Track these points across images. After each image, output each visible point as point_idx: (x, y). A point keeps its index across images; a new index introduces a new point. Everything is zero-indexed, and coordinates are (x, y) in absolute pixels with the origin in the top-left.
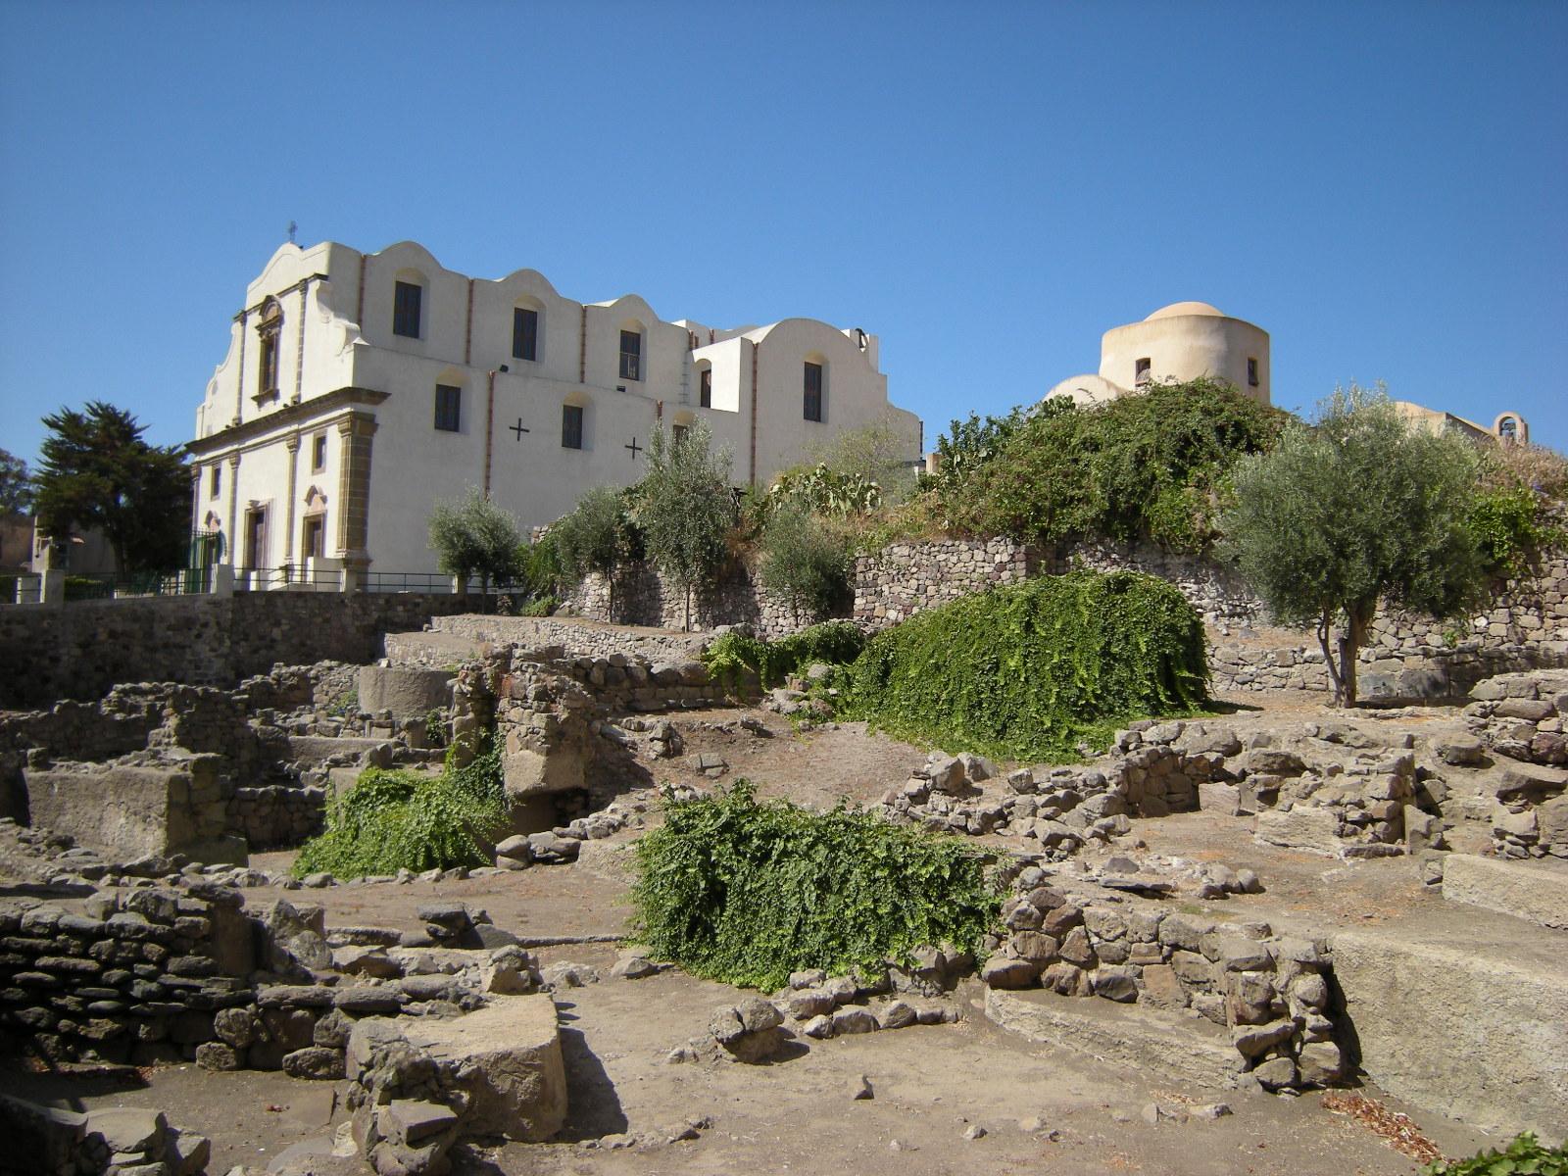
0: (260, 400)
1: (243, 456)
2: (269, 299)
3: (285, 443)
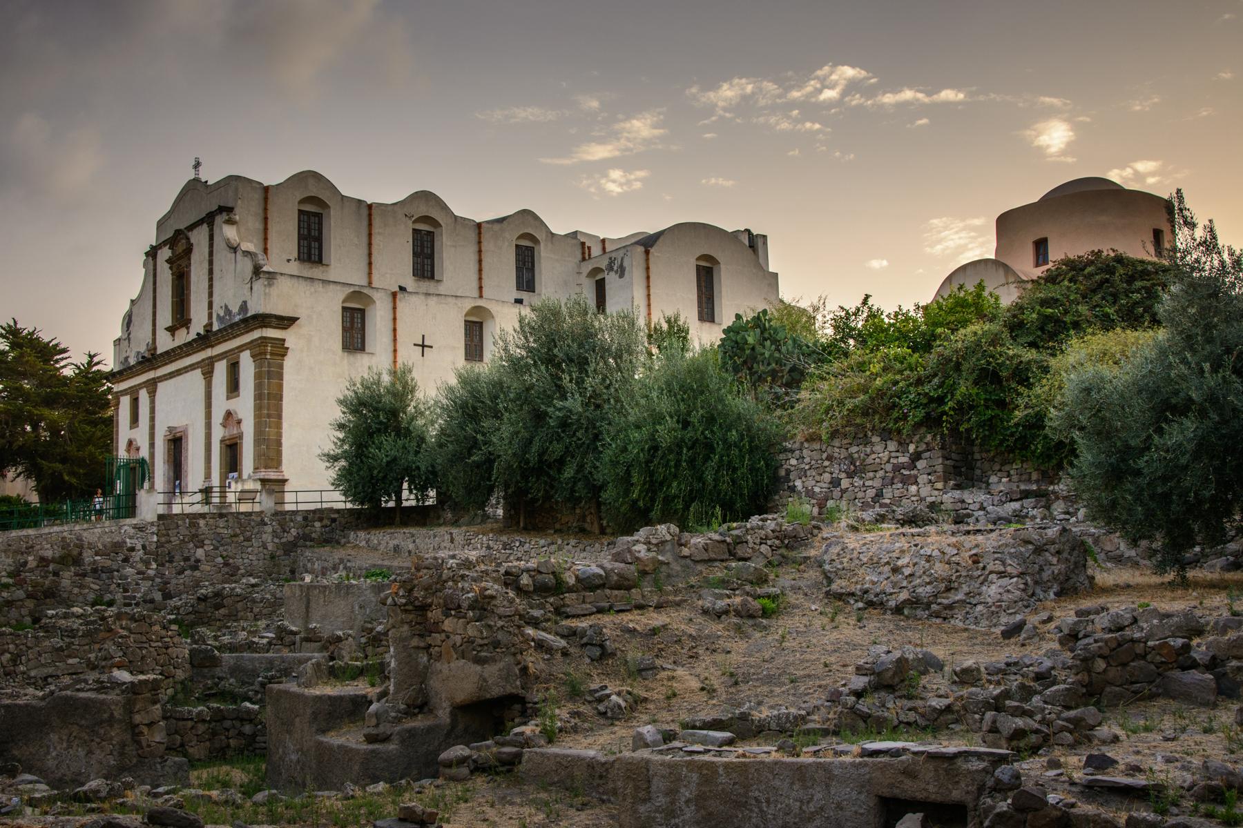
0: (172, 330)
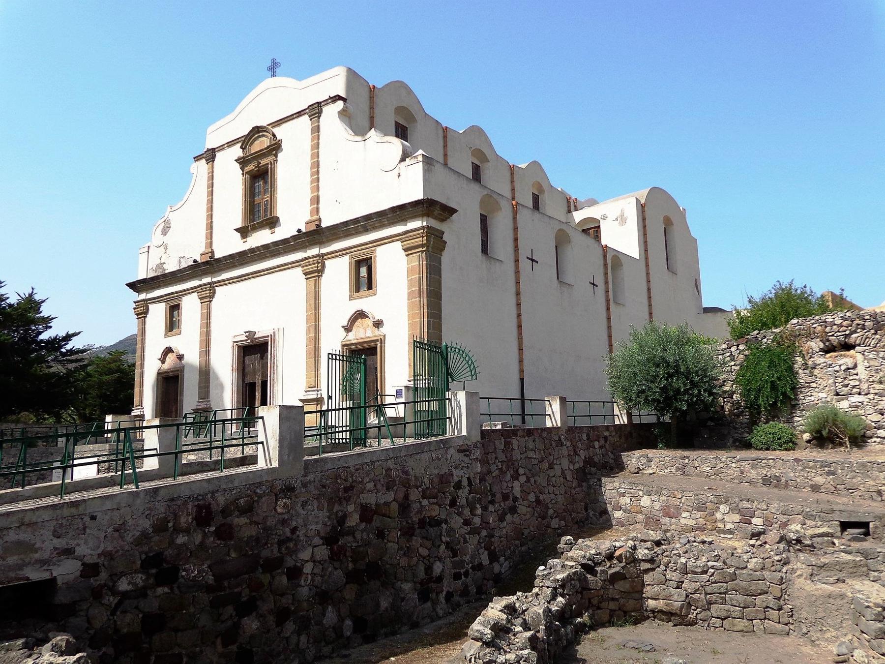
1: (328, 263)
3: (299, 269)
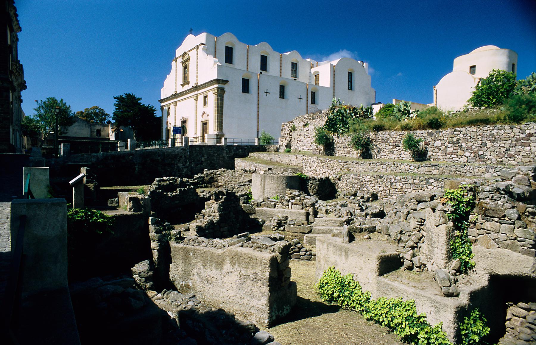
0: (183, 85)
2: (185, 53)
